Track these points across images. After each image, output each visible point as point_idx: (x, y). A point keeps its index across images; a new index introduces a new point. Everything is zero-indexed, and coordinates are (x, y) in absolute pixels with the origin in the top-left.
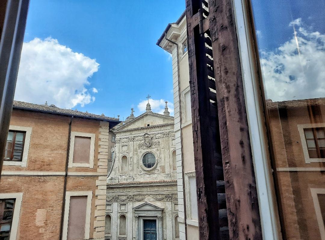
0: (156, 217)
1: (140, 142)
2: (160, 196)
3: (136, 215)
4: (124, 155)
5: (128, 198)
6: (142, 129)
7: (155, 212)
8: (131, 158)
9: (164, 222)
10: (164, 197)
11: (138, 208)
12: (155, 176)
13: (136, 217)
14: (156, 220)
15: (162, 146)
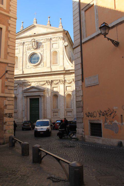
0: (39, 96)
1: (28, 46)
3: (25, 95)
4: (54, 51)
5: (18, 84)
6: (31, 36)
7: (39, 93)
8: (21, 57)
9: (45, 99)
10: (45, 83)
11: (26, 90)
12: (40, 69)
13: (24, 97)
14: (39, 98)
15: (44, 48)
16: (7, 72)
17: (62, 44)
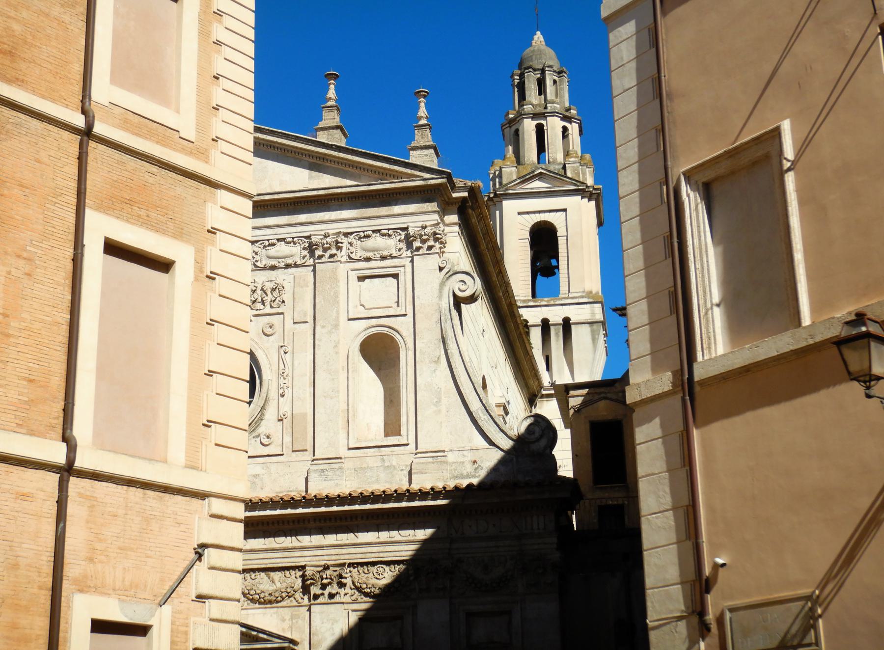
2: (276, 576)
16: (200, 551)
17: (436, 286)
